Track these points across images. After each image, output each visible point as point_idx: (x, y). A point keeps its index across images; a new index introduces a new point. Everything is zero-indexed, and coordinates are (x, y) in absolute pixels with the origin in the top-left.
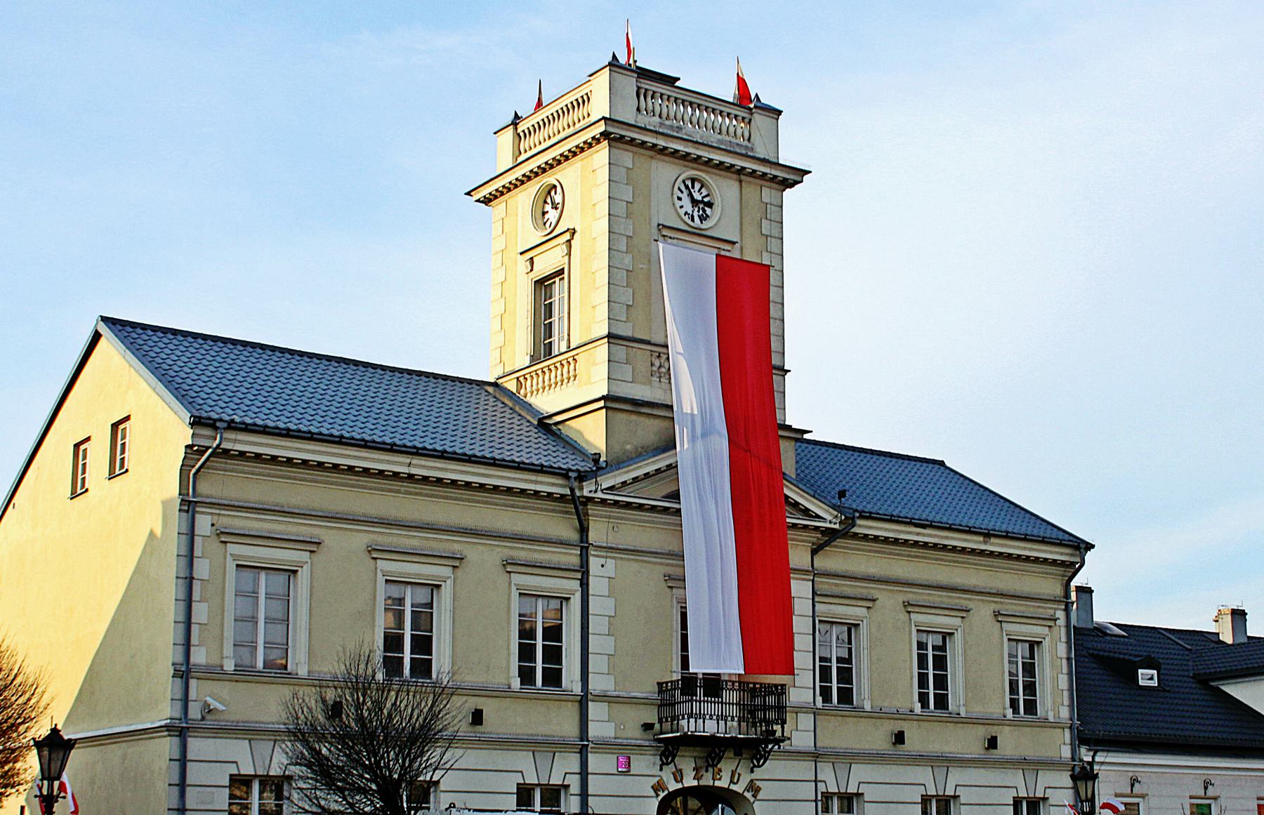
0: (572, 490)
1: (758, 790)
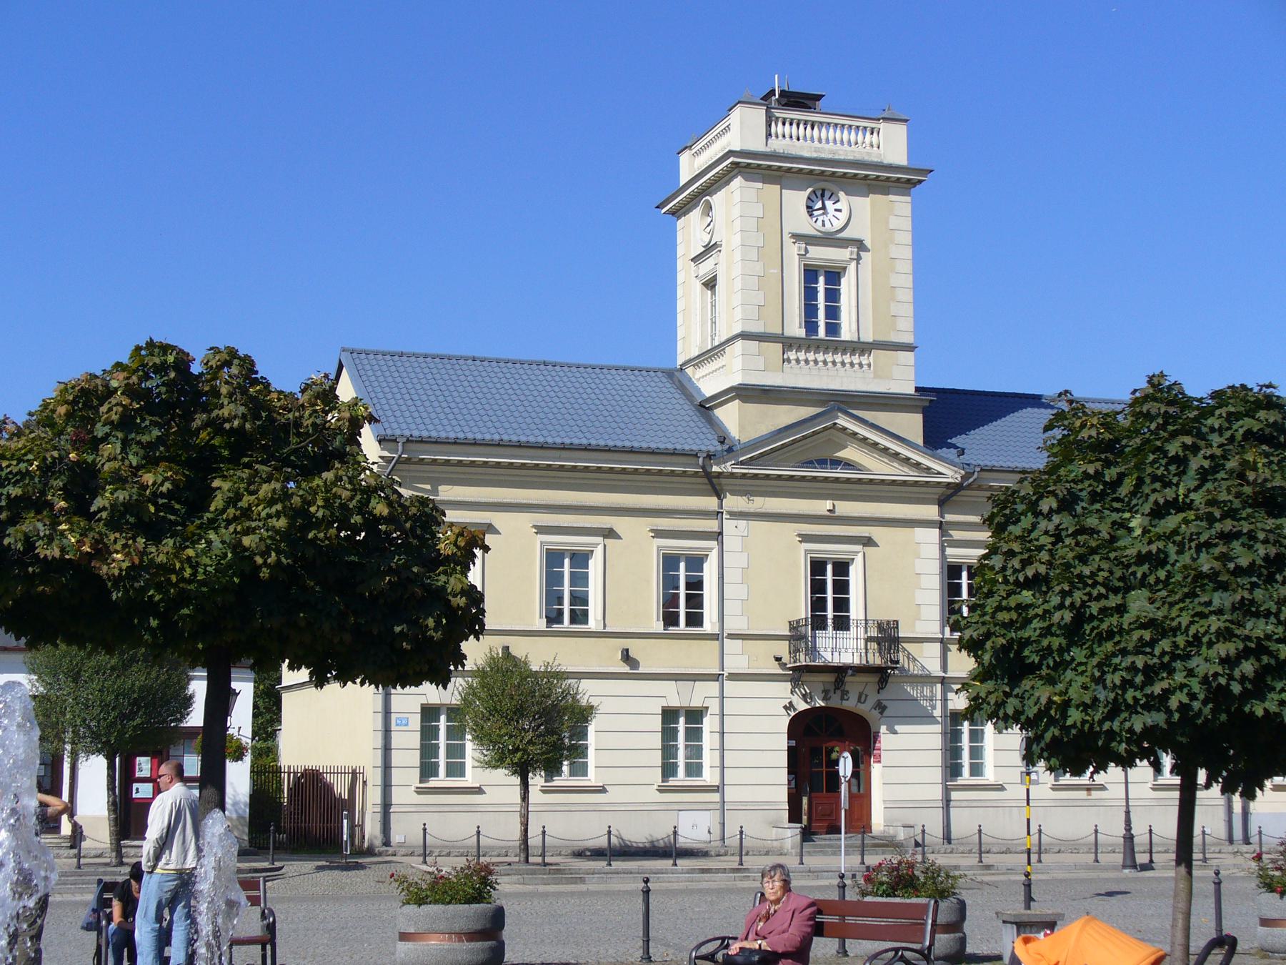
0: (703, 467)
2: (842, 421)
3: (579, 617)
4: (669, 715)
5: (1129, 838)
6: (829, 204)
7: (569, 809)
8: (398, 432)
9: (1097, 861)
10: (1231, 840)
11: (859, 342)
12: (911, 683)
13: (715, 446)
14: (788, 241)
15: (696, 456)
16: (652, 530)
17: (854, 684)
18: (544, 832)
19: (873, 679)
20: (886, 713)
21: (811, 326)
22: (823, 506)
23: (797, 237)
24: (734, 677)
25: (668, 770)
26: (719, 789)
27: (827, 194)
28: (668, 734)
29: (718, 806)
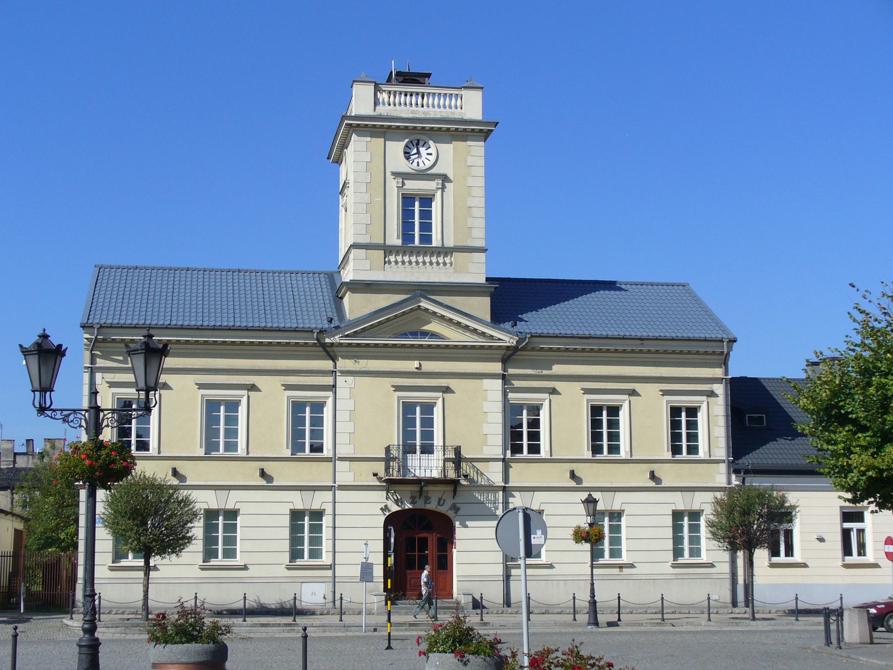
0: (317, 339)
2: (424, 304)
4: (677, 515)
5: (593, 603)
6: (422, 150)
7: (220, 582)
8: (313, 326)
9: (575, 620)
10: (734, 604)
11: (443, 247)
12: (479, 491)
14: (389, 176)
15: (92, 327)
17: (435, 493)
20: (459, 513)
21: (407, 236)
23: (396, 174)
24: (343, 488)
26: (332, 567)
27: (421, 143)
28: (677, 528)
29: (331, 580)
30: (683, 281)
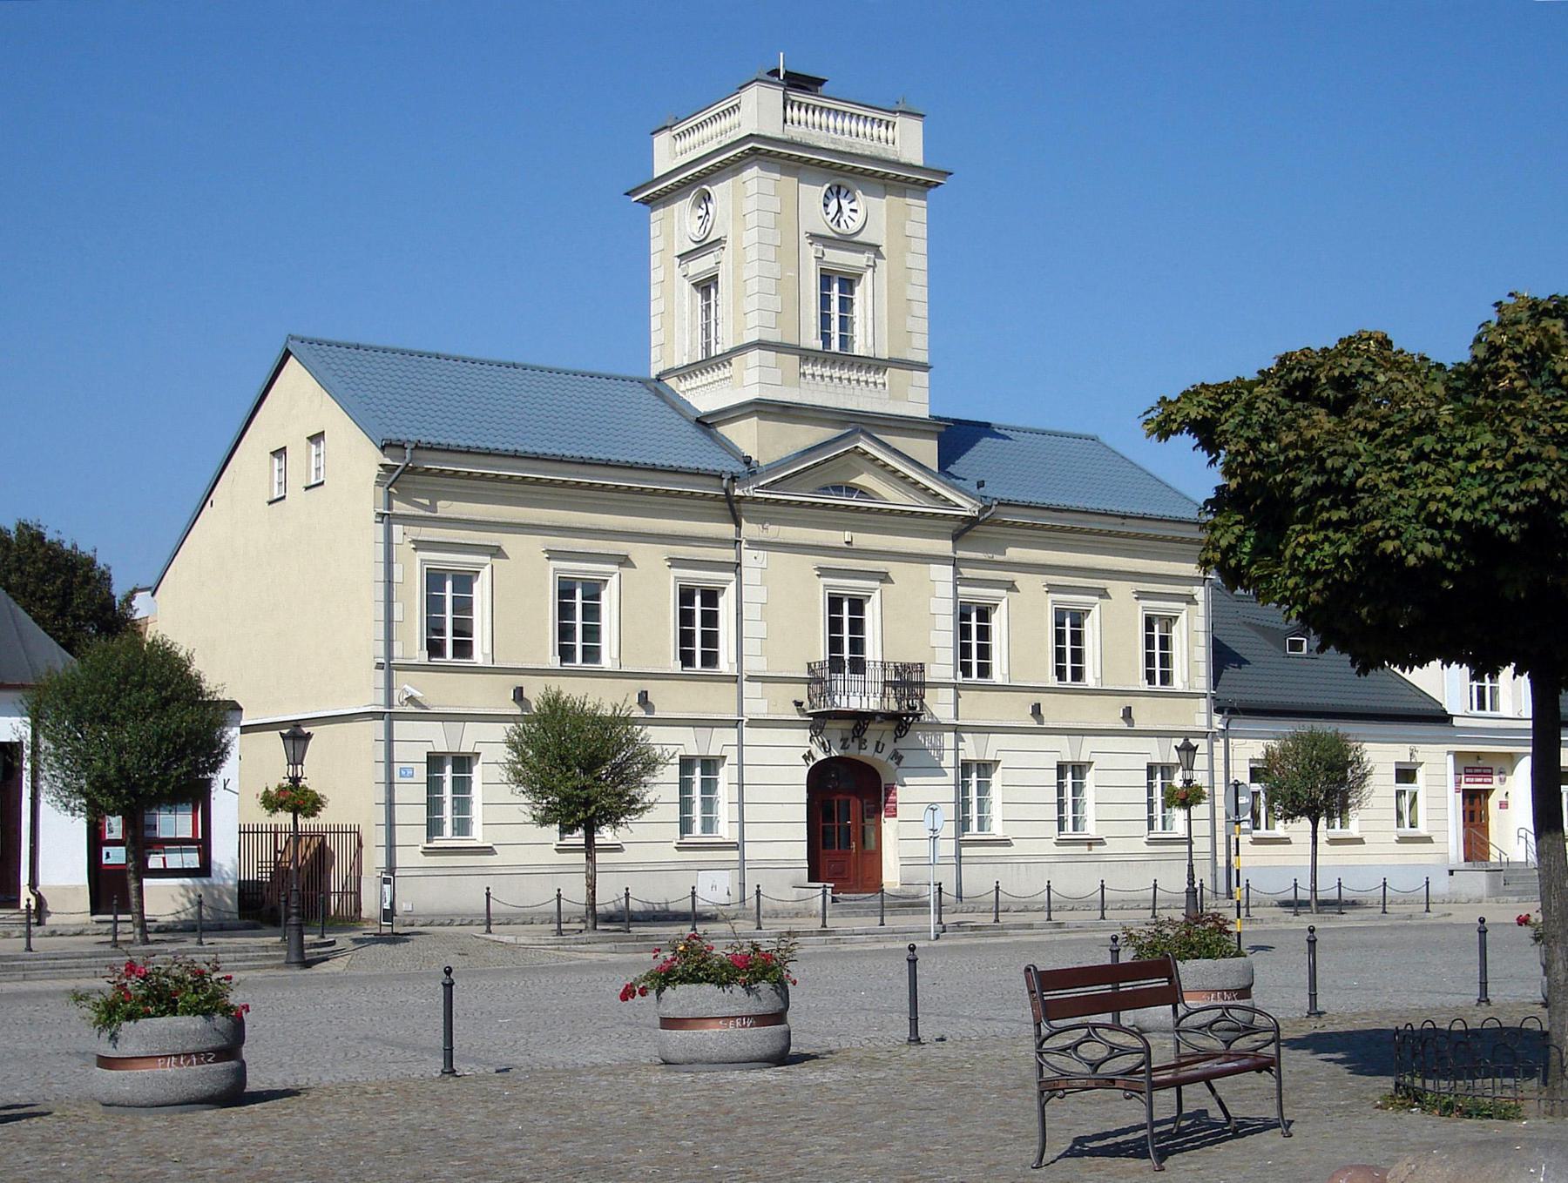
0: (726, 491)
1: (901, 758)
2: (864, 445)
3: (463, 648)
4: (435, 762)
9: (29, 949)
13: (740, 468)
14: (805, 241)
15: (403, 447)
16: (670, 559)
18: (559, 896)
19: (891, 726)
21: (826, 338)
22: (838, 538)
24: (755, 723)
25: (685, 826)
26: (738, 846)
27: (843, 192)
30: (1091, 433)
